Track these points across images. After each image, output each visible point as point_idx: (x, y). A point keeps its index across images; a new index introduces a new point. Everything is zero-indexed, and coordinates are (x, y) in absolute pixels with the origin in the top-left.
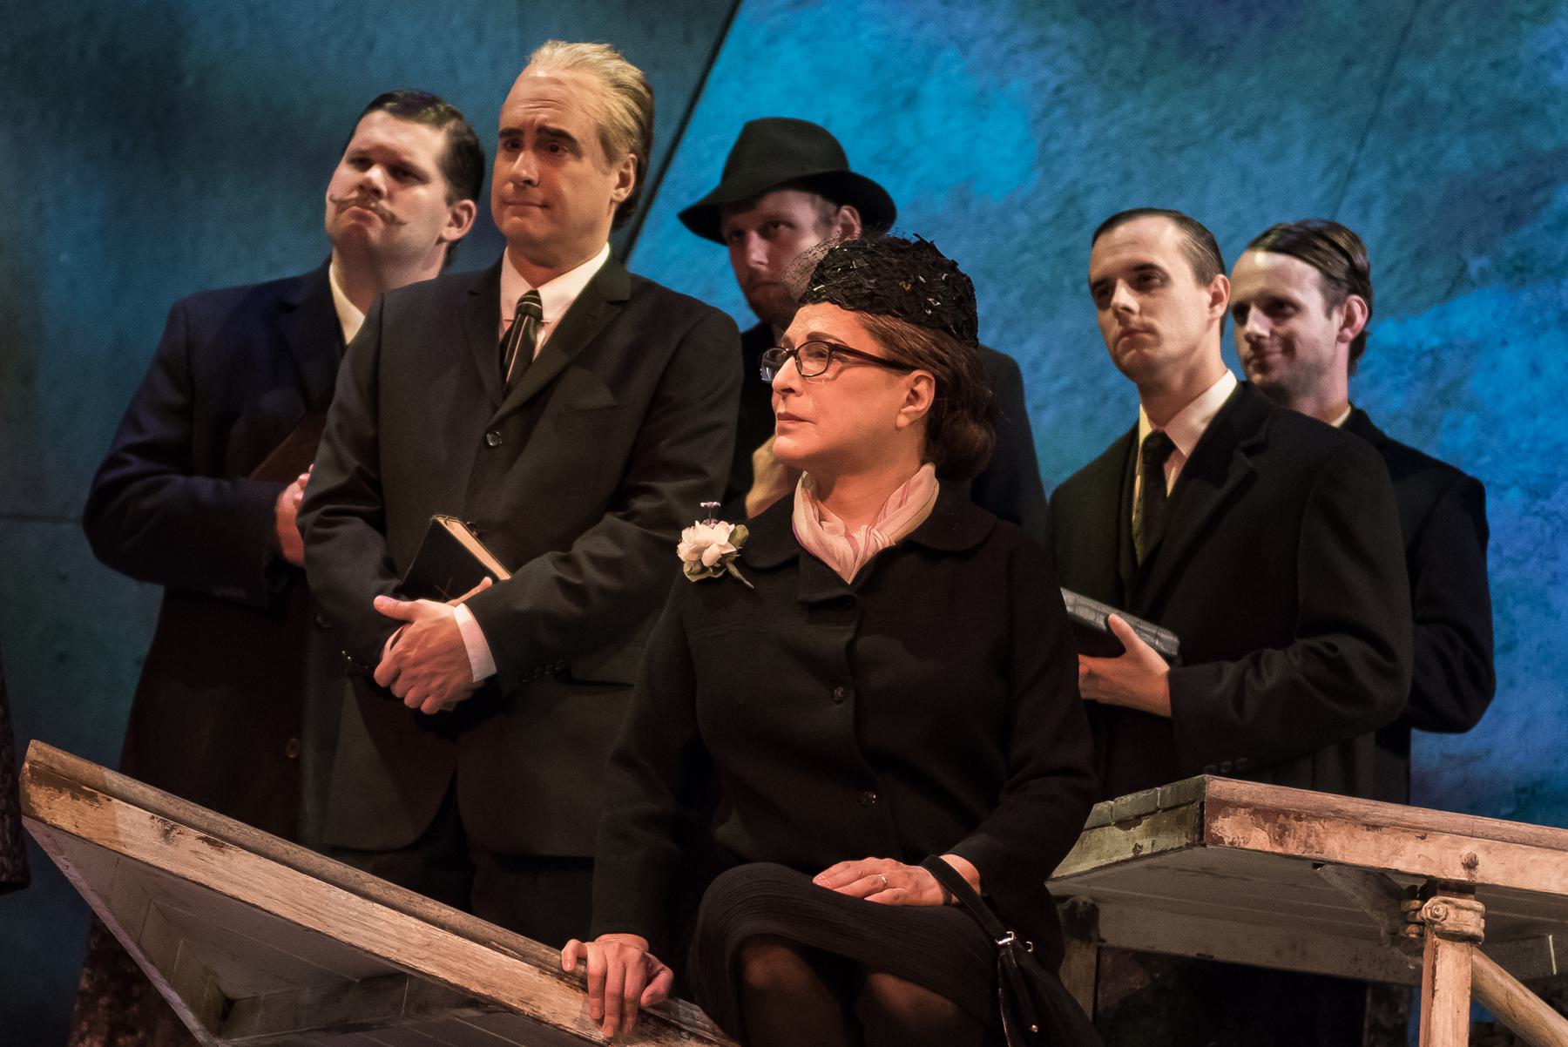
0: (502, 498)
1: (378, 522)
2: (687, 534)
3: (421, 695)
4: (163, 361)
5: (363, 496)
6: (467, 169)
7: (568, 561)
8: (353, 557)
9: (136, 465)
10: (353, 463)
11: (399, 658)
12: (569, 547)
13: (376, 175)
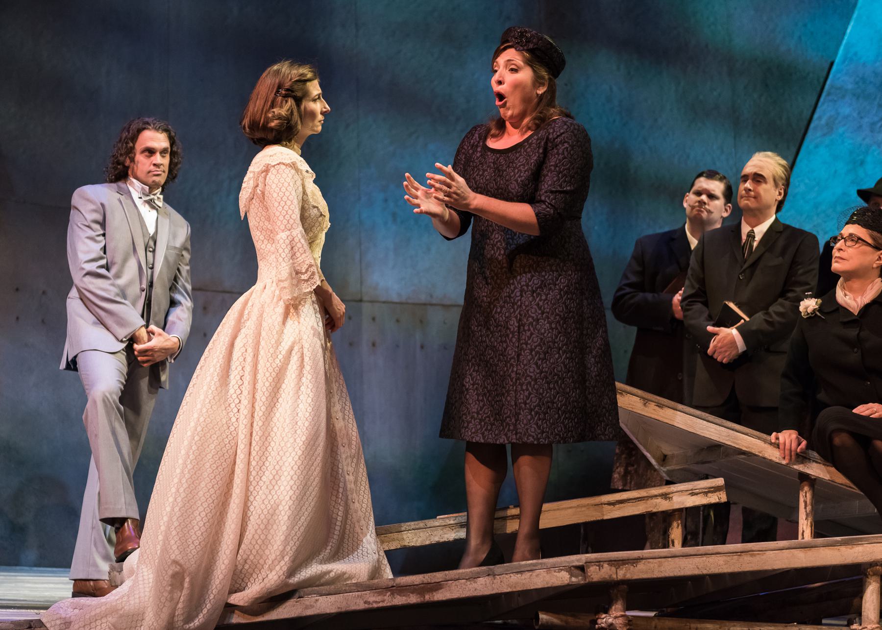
0: (746, 294)
1: (706, 304)
2: (802, 303)
3: (723, 357)
4: (634, 257)
5: (701, 296)
6: (729, 194)
7: (767, 314)
8: (698, 317)
9: (628, 290)
10: (697, 286)
11: (715, 347)
12: (767, 309)
13: (704, 197)
